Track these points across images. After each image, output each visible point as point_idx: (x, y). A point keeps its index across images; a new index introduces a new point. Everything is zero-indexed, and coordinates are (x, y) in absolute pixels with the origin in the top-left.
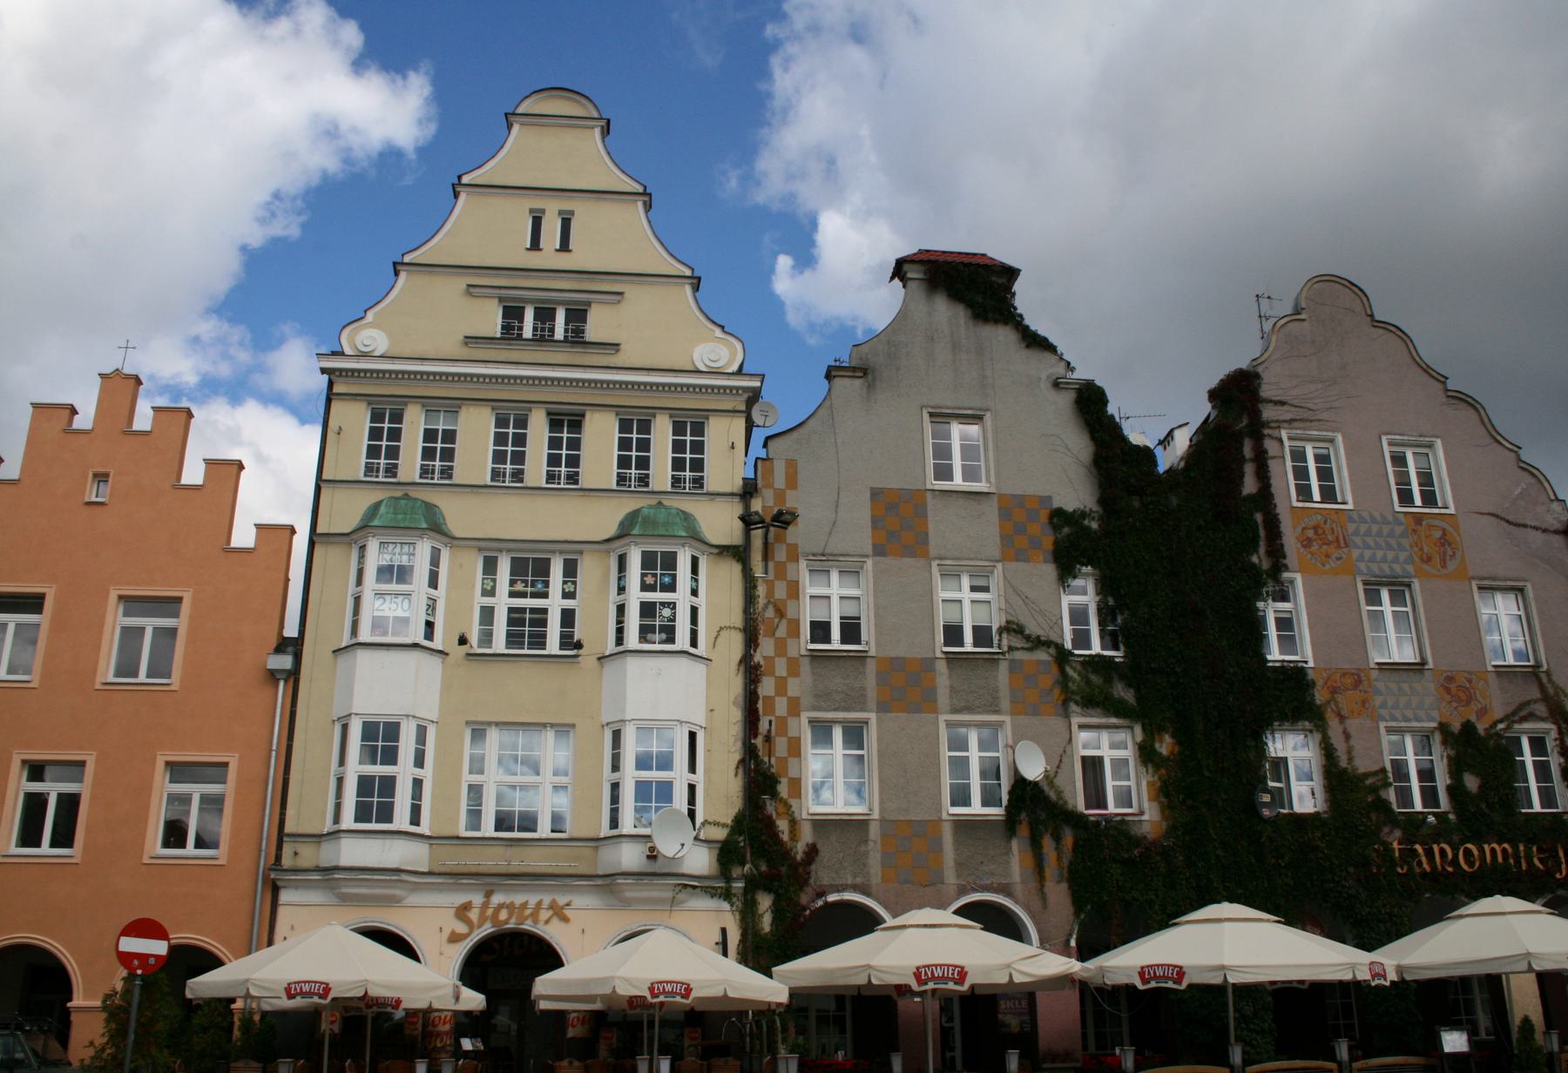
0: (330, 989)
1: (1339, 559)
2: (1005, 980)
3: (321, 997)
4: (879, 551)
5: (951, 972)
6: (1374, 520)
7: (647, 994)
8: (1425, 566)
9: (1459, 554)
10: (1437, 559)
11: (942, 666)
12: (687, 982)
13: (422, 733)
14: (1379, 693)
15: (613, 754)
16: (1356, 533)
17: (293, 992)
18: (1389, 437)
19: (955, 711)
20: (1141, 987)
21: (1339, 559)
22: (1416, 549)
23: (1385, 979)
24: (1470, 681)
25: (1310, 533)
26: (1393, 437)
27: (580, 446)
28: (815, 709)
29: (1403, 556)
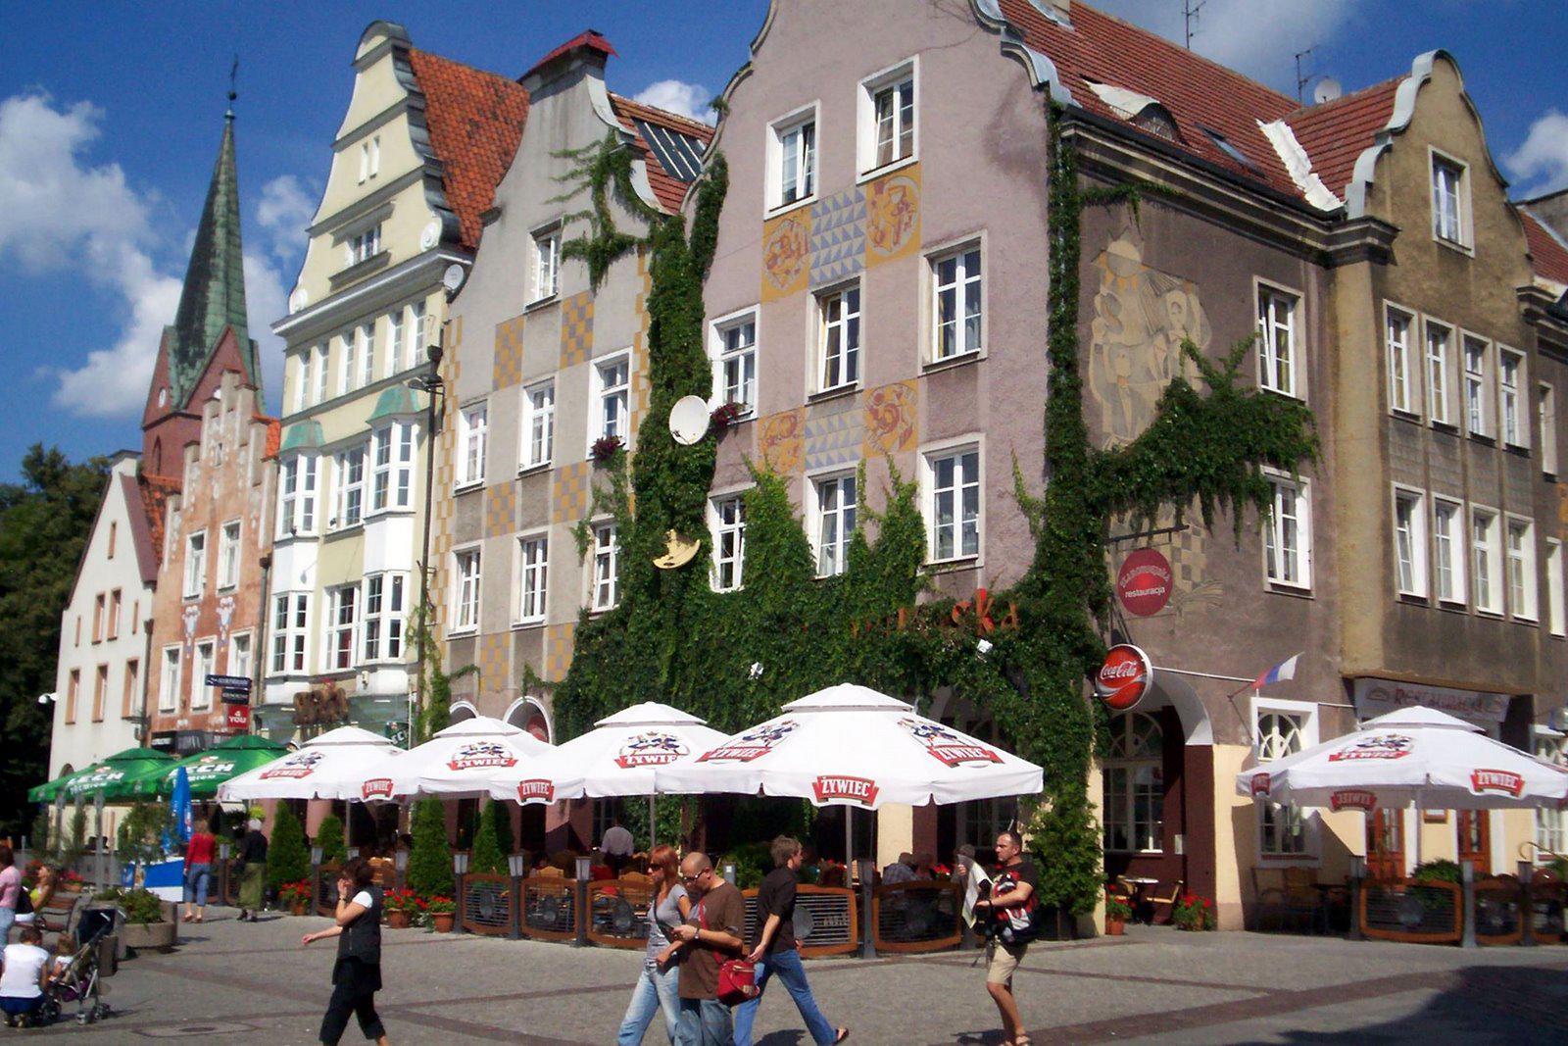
0: (877, 790)
2: (754, 791)
3: (1513, 794)
5: (857, 787)
6: (848, 202)
7: (1469, 785)
8: (879, 250)
9: (914, 219)
10: (890, 237)
11: (922, 387)
12: (870, 778)
13: (302, 605)
14: (809, 434)
15: (284, 651)
16: (818, 231)
17: (825, 791)
19: (524, 527)
20: (815, 803)
24: (899, 396)
25: (777, 249)
27: (55, 685)
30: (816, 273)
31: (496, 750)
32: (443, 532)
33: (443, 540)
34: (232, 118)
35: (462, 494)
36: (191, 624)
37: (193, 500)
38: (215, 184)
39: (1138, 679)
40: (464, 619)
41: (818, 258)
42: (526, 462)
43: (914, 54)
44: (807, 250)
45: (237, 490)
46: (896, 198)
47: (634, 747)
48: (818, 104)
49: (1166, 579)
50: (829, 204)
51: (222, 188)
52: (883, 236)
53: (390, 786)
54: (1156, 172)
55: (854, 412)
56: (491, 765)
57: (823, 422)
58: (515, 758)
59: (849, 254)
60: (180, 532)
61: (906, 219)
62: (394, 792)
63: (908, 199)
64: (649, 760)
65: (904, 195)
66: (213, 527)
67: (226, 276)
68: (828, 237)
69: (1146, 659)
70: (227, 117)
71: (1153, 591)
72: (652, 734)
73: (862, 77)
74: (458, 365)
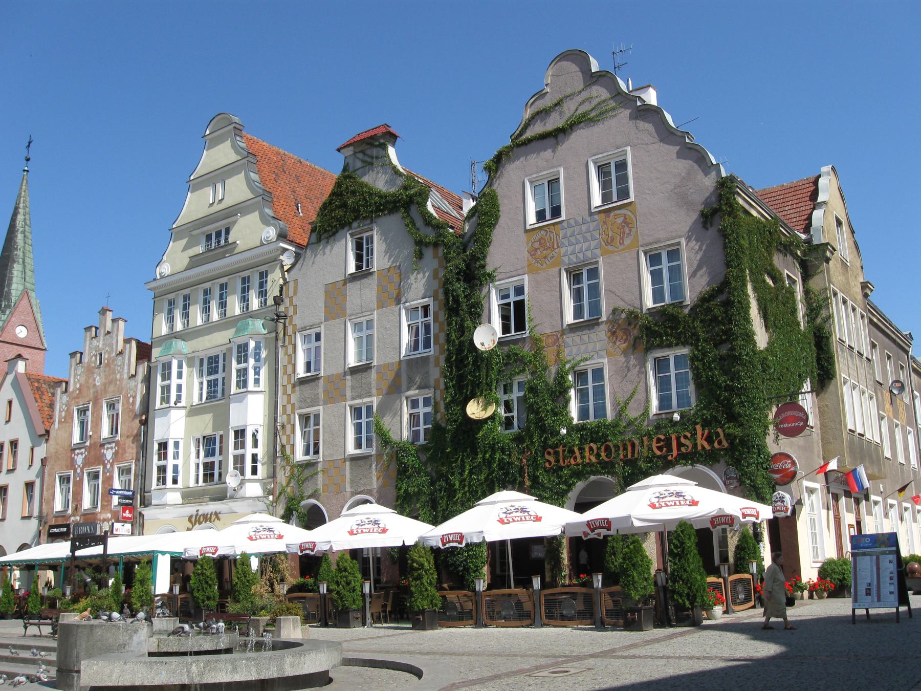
1: (552, 257)
3: (214, 554)
4: (326, 320)
8: (609, 248)
13: (176, 444)
18: (594, 158)
19: (353, 399)
21: (552, 257)
22: (604, 236)
23: (757, 518)
25: (537, 245)
26: (596, 157)
28: (300, 408)
29: (593, 244)
30: (566, 259)
31: (376, 522)
32: (289, 401)
33: (289, 407)
34: (28, 171)
35: (303, 382)
36: (79, 460)
37: (78, 386)
38: (16, 209)
39: (793, 469)
40: (358, 445)
41: (567, 250)
42: (352, 361)
43: (626, 146)
44: (558, 247)
45: (116, 380)
46: (620, 220)
47: (505, 513)
48: (561, 170)
49: (804, 418)
50: (572, 222)
51: (21, 211)
52: (613, 239)
53: (314, 546)
54: (759, 213)
55: (599, 334)
56: (680, 505)
57: (577, 339)
58: (387, 528)
59: (588, 249)
60: (68, 405)
61: (627, 231)
62: (316, 550)
63: (628, 220)
64: (516, 520)
65: (625, 218)
66: (96, 401)
67: (24, 262)
68: (573, 240)
69: (794, 459)
70: (24, 170)
71: (796, 424)
72: (368, 518)
73: (592, 156)
74: (295, 307)
